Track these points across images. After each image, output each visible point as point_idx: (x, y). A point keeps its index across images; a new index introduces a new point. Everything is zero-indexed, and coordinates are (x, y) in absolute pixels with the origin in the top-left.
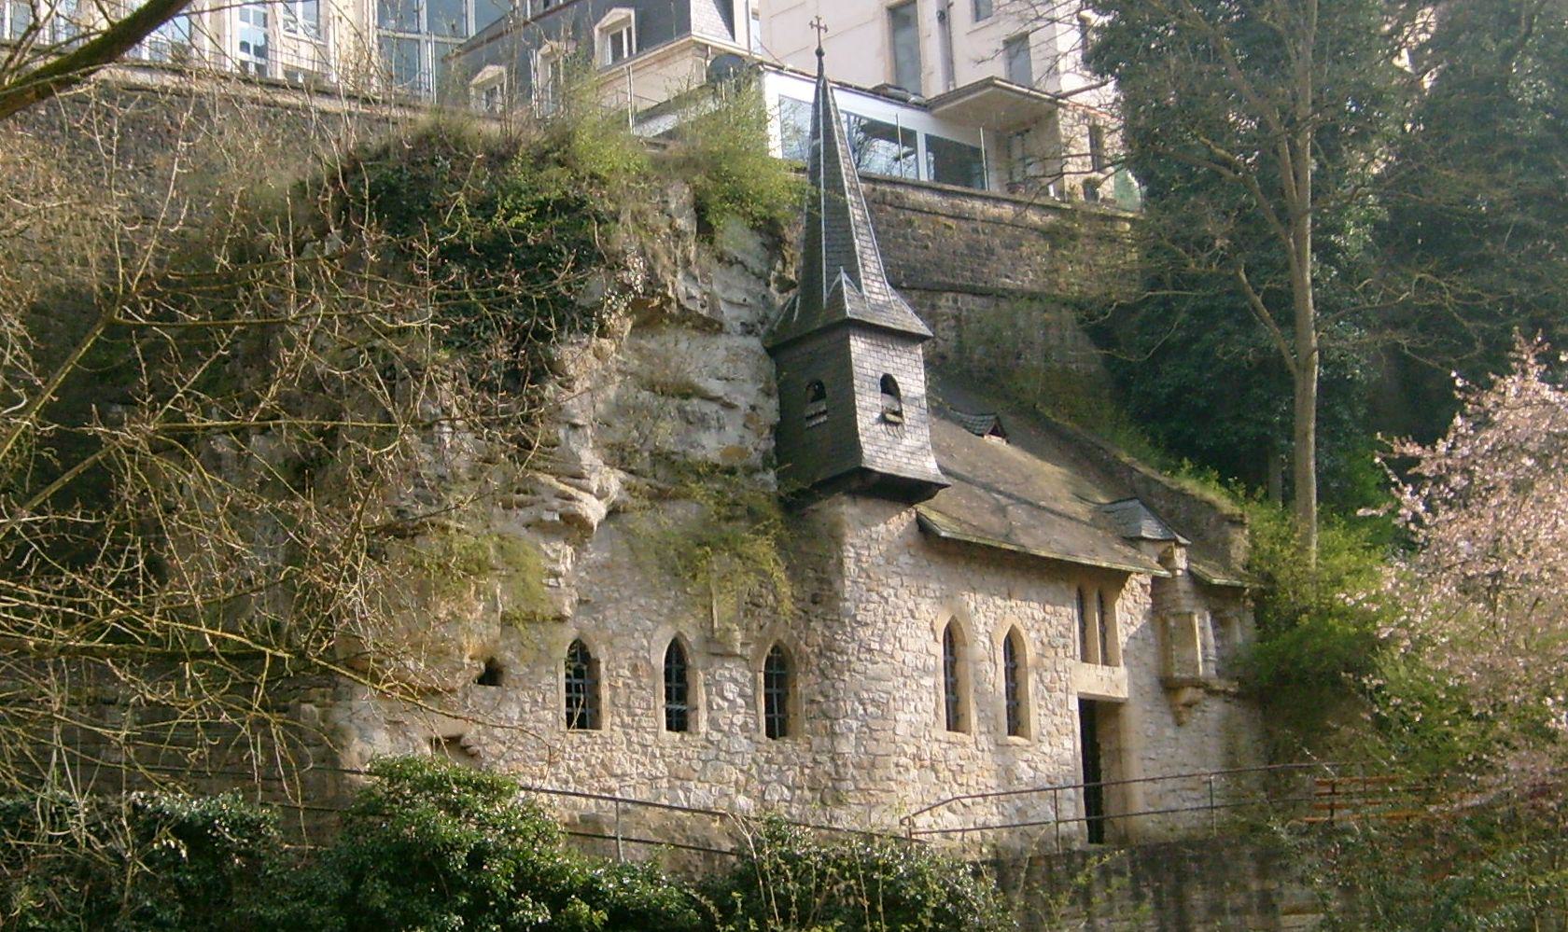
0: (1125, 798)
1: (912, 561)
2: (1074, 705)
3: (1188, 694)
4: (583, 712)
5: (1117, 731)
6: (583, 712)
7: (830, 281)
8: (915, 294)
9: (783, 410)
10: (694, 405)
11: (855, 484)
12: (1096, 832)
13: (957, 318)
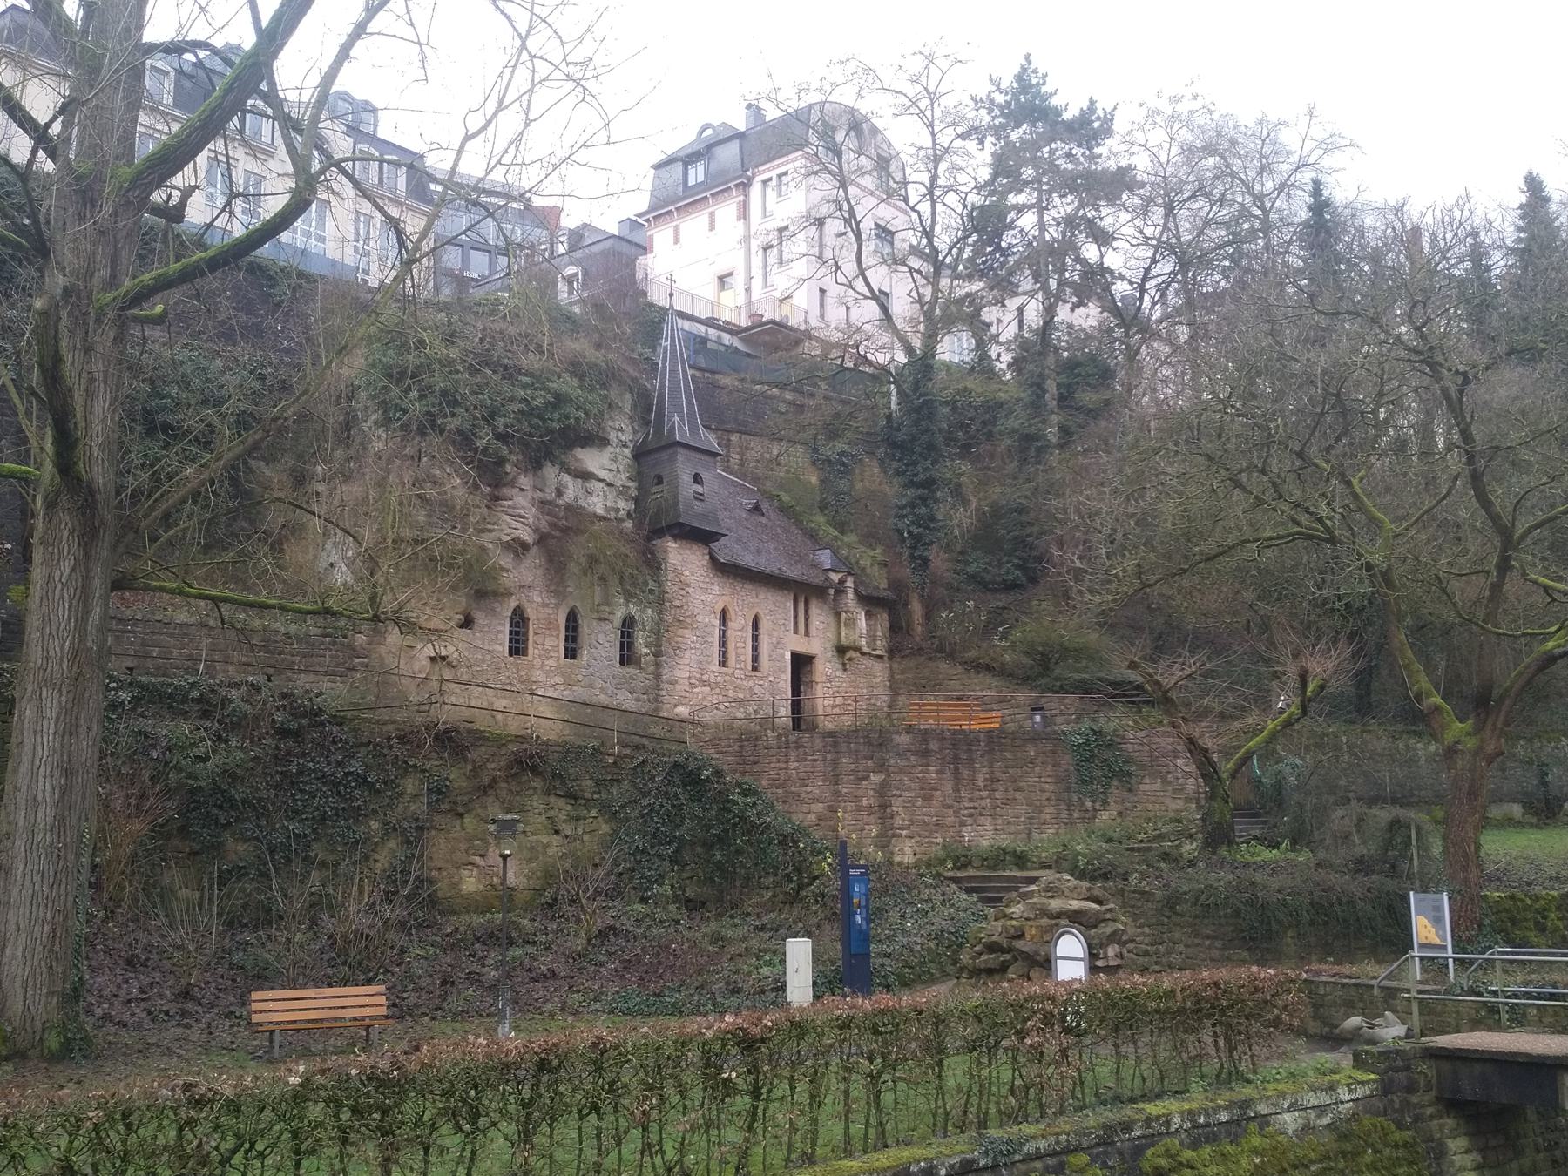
0: (814, 708)
2: (788, 656)
3: (851, 654)
4: (518, 647)
5: (811, 672)
6: (518, 647)
9: (639, 489)
12: (797, 723)
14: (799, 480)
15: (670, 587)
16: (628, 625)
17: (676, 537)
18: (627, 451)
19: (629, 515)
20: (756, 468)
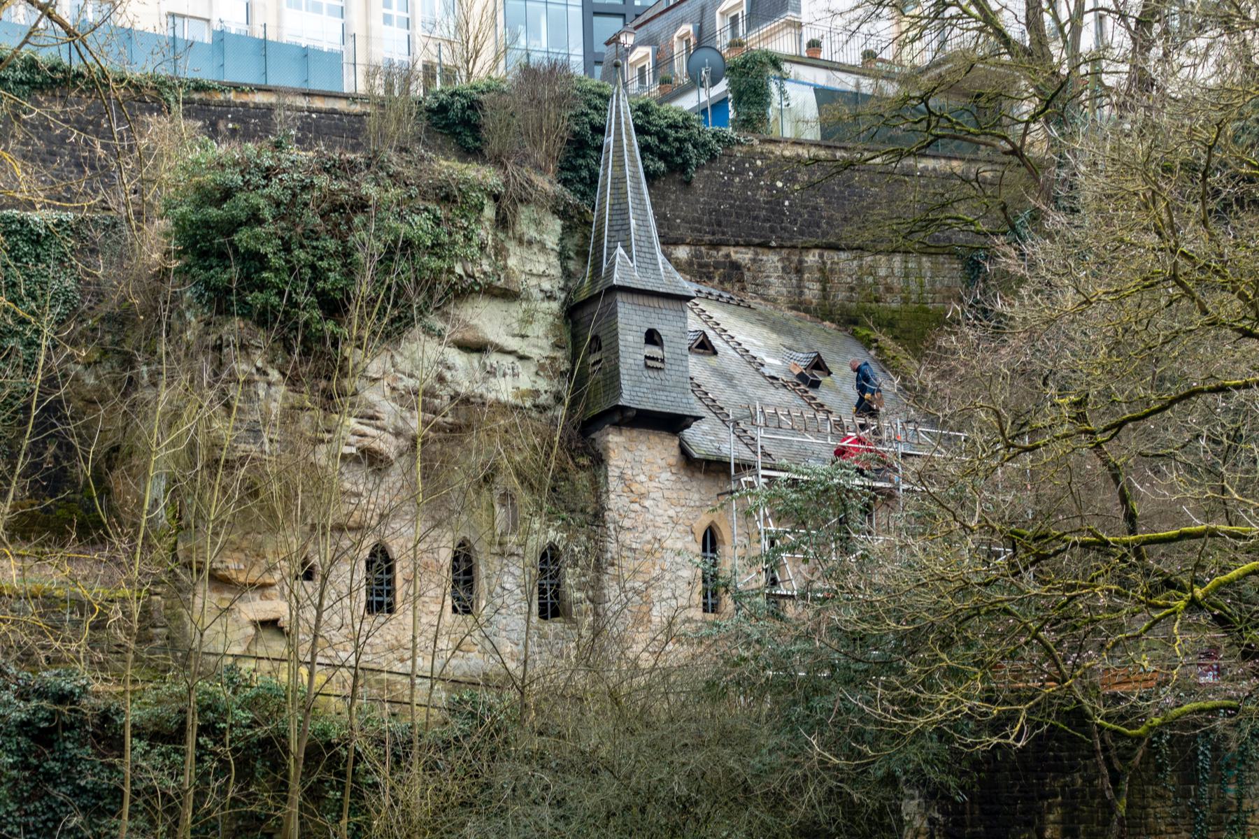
1: (673, 478)
7: (609, 254)
8: (784, 252)
10: (493, 359)
11: (617, 418)
13: (821, 270)
14: (927, 311)
15: (616, 501)
16: (550, 556)
17: (619, 425)
18: (555, 306)
19: (558, 398)
20: (850, 300)
